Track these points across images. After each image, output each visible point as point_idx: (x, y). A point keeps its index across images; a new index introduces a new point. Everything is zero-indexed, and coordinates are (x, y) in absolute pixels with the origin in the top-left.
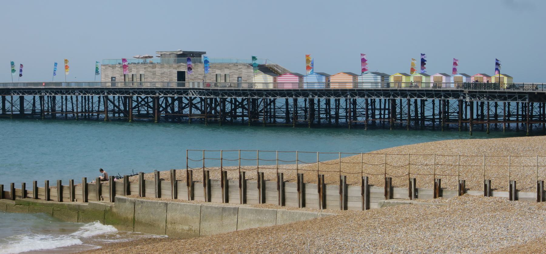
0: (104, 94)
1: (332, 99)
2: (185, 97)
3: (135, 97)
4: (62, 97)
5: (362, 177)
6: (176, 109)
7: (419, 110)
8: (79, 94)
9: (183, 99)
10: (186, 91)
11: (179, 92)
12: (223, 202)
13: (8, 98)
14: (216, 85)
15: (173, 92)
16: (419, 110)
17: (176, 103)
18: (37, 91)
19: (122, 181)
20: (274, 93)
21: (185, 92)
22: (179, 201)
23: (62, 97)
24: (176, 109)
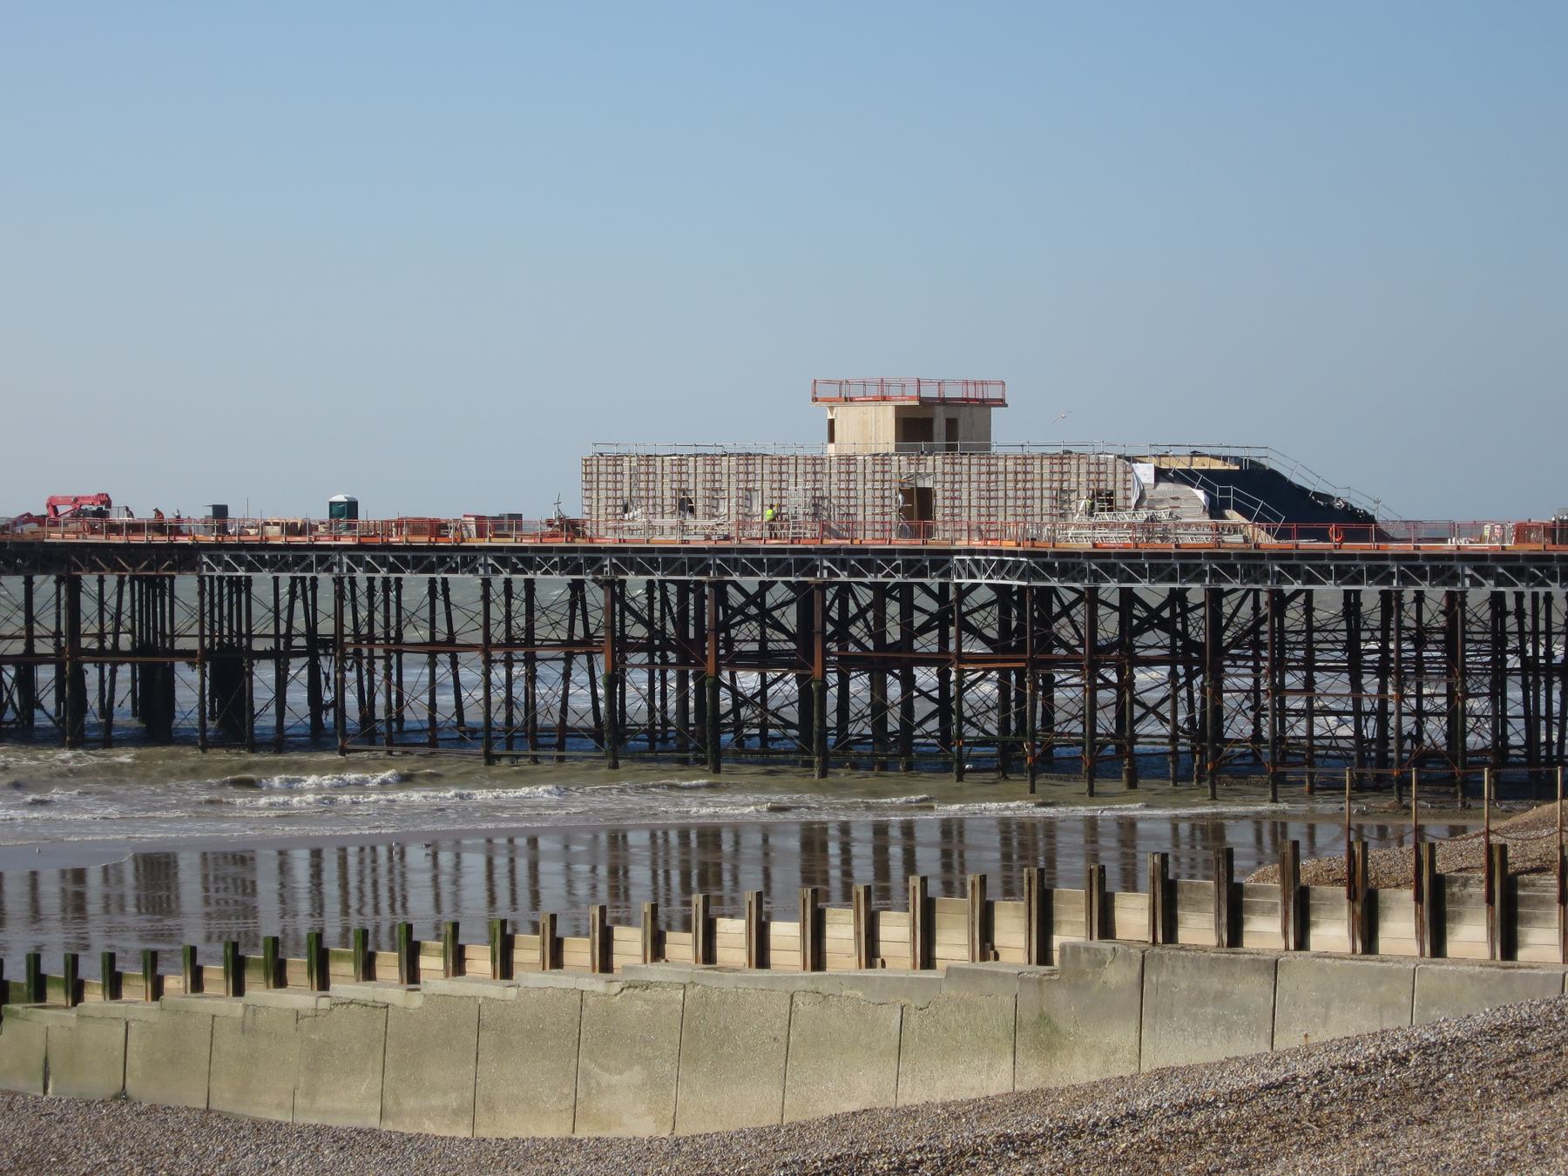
0: (600, 571)
1: (45, 585)
2: (922, 585)
3: (1110, 589)
4: (276, 579)
5: (659, 984)
6: (894, 634)
7: (658, 685)
8: (496, 571)
9: (917, 591)
10: (940, 560)
11: (914, 563)
12: (914, 966)
13: (89, 581)
14: (742, 525)
15: (546, 560)
16: (658, 685)
17: (893, 608)
18: (313, 556)
19: (504, 841)
20: (752, 561)
21: (935, 566)
22: (1183, 948)
23: (276, 579)
24: (894, 634)
